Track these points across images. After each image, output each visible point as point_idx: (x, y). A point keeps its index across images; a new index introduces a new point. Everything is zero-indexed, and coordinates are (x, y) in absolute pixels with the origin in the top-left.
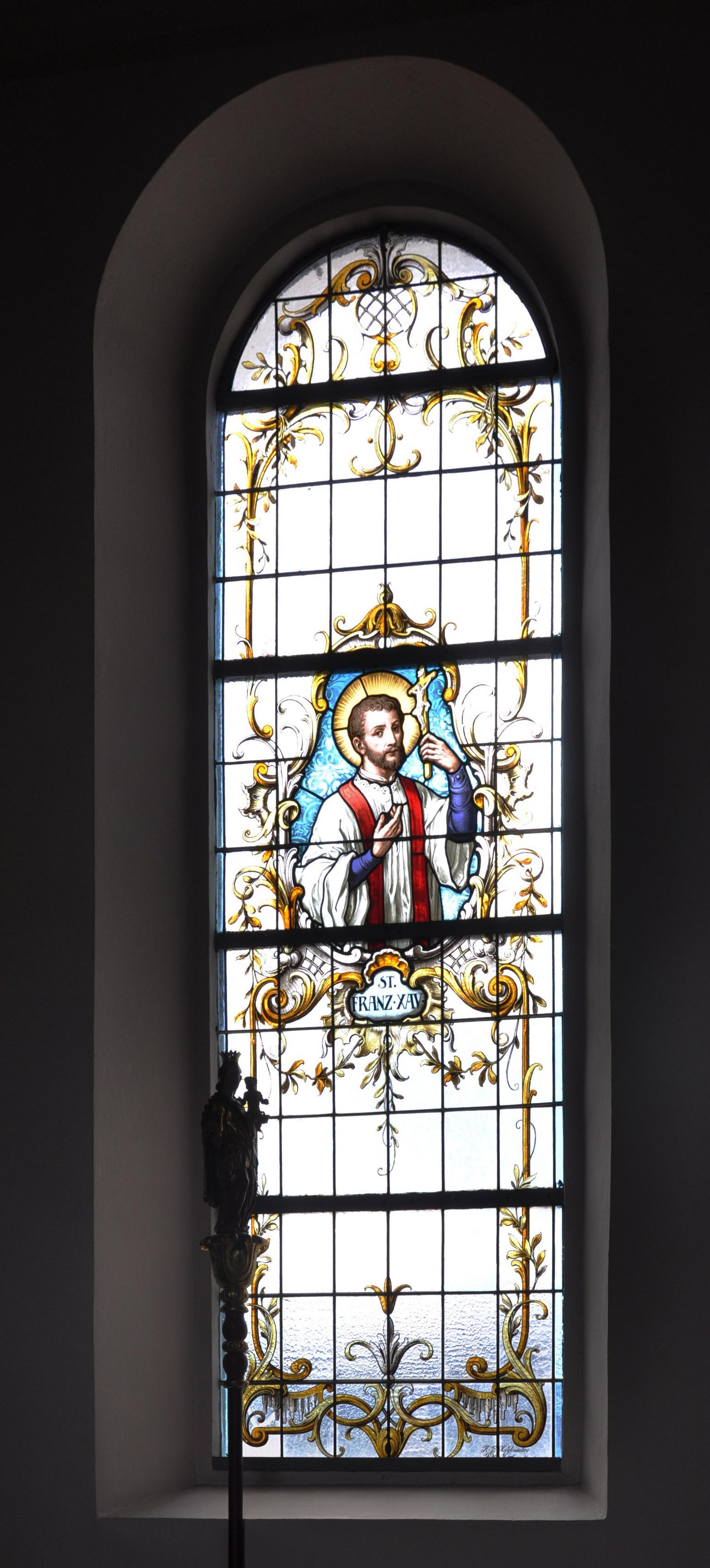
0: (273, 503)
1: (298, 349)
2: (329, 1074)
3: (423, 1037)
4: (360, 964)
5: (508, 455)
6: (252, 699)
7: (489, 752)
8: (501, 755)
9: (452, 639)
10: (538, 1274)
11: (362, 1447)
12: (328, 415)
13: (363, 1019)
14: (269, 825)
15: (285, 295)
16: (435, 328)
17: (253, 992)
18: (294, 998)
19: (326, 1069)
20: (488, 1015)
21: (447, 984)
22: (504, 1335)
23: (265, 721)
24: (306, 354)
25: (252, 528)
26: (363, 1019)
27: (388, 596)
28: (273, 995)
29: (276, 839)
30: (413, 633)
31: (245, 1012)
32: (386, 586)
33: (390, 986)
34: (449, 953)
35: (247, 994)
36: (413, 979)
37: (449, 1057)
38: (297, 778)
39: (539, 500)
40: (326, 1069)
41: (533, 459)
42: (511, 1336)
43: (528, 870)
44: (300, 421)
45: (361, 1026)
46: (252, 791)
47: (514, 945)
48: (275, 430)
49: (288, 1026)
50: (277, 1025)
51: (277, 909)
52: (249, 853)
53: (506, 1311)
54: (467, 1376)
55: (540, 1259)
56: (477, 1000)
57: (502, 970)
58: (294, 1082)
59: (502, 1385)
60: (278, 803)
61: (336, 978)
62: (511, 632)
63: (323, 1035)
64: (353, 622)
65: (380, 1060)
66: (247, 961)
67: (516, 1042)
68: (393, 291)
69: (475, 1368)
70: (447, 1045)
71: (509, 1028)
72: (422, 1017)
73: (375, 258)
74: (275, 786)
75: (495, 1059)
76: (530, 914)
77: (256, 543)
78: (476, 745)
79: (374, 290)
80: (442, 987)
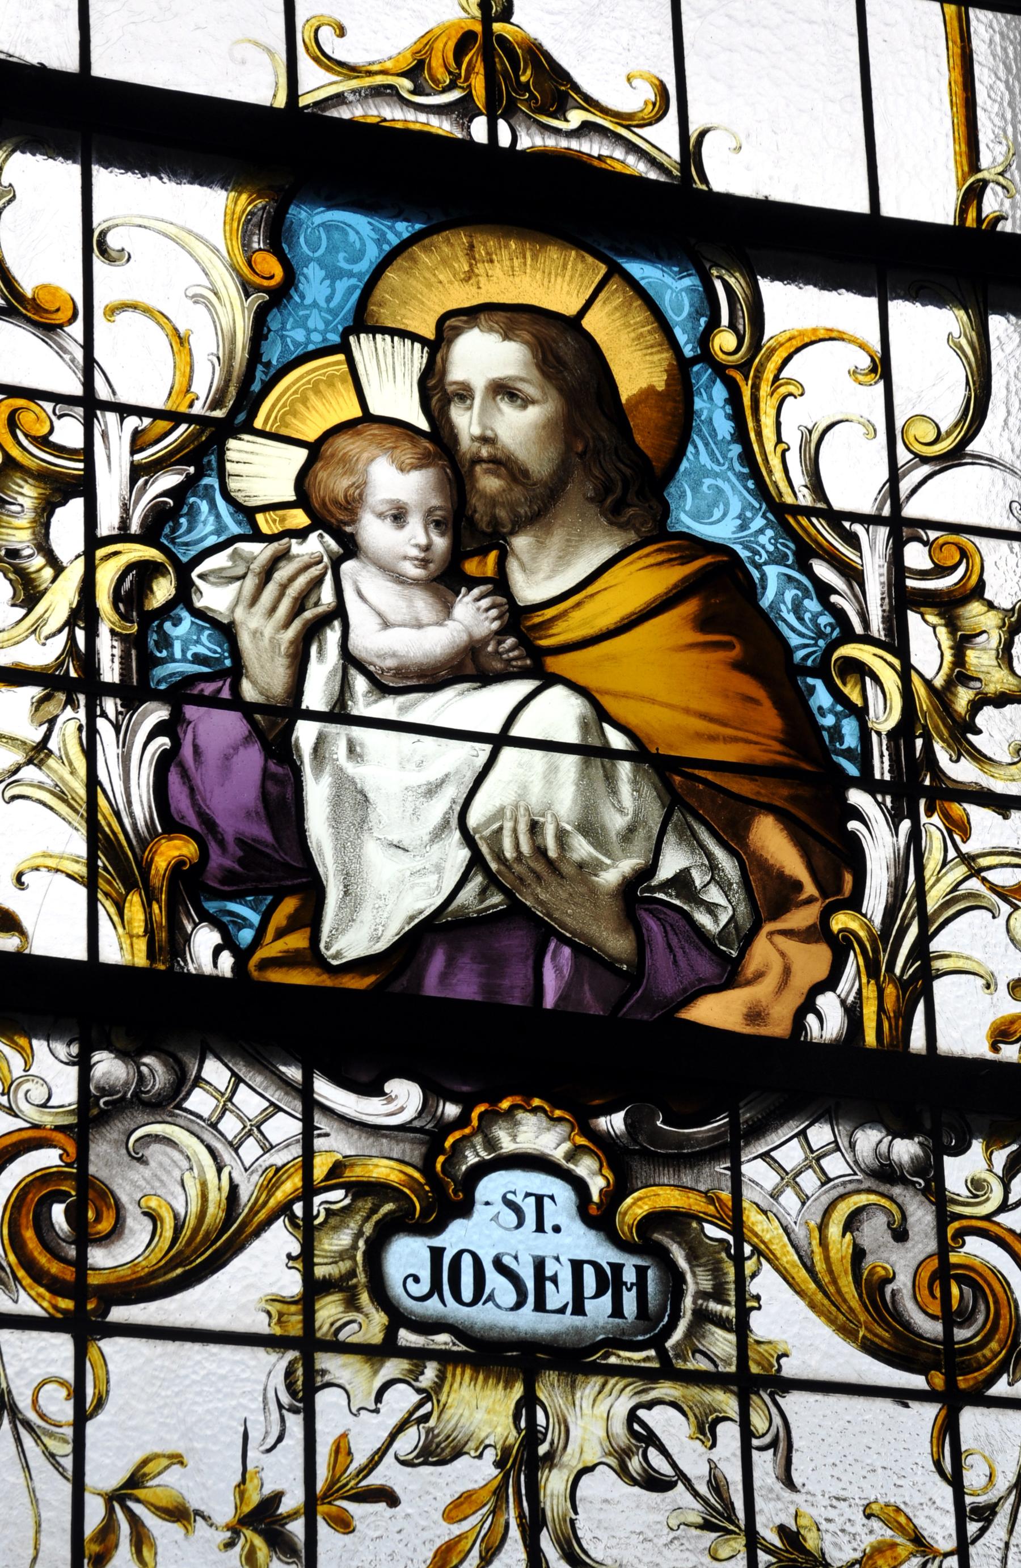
2: (292, 1516)
3: (663, 1421)
7: (874, 544)
8: (916, 556)
9: (727, 174)
14: (61, 598)
18: (153, 1216)
19: (277, 1498)
20: (917, 1382)
21: (756, 1251)
26: (427, 1327)
28: (59, 1196)
29: (89, 661)
30: (586, 129)
33: (540, 1228)
36: (636, 1207)
37: (772, 1513)
38: (168, 480)
40: (277, 1498)
45: (418, 1356)
49: (119, 1314)
51: (91, 883)
56: (870, 1315)
57: (961, 1234)
58: (140, 1538)
60: (93, 542)
61: (321, 1168)
63: (269, 1368)
65: (502, 1487)
72: (662, 1354)
74: (85, 487)
75: (951, 1544)
78: (835, 518)
80: (739, 1260)
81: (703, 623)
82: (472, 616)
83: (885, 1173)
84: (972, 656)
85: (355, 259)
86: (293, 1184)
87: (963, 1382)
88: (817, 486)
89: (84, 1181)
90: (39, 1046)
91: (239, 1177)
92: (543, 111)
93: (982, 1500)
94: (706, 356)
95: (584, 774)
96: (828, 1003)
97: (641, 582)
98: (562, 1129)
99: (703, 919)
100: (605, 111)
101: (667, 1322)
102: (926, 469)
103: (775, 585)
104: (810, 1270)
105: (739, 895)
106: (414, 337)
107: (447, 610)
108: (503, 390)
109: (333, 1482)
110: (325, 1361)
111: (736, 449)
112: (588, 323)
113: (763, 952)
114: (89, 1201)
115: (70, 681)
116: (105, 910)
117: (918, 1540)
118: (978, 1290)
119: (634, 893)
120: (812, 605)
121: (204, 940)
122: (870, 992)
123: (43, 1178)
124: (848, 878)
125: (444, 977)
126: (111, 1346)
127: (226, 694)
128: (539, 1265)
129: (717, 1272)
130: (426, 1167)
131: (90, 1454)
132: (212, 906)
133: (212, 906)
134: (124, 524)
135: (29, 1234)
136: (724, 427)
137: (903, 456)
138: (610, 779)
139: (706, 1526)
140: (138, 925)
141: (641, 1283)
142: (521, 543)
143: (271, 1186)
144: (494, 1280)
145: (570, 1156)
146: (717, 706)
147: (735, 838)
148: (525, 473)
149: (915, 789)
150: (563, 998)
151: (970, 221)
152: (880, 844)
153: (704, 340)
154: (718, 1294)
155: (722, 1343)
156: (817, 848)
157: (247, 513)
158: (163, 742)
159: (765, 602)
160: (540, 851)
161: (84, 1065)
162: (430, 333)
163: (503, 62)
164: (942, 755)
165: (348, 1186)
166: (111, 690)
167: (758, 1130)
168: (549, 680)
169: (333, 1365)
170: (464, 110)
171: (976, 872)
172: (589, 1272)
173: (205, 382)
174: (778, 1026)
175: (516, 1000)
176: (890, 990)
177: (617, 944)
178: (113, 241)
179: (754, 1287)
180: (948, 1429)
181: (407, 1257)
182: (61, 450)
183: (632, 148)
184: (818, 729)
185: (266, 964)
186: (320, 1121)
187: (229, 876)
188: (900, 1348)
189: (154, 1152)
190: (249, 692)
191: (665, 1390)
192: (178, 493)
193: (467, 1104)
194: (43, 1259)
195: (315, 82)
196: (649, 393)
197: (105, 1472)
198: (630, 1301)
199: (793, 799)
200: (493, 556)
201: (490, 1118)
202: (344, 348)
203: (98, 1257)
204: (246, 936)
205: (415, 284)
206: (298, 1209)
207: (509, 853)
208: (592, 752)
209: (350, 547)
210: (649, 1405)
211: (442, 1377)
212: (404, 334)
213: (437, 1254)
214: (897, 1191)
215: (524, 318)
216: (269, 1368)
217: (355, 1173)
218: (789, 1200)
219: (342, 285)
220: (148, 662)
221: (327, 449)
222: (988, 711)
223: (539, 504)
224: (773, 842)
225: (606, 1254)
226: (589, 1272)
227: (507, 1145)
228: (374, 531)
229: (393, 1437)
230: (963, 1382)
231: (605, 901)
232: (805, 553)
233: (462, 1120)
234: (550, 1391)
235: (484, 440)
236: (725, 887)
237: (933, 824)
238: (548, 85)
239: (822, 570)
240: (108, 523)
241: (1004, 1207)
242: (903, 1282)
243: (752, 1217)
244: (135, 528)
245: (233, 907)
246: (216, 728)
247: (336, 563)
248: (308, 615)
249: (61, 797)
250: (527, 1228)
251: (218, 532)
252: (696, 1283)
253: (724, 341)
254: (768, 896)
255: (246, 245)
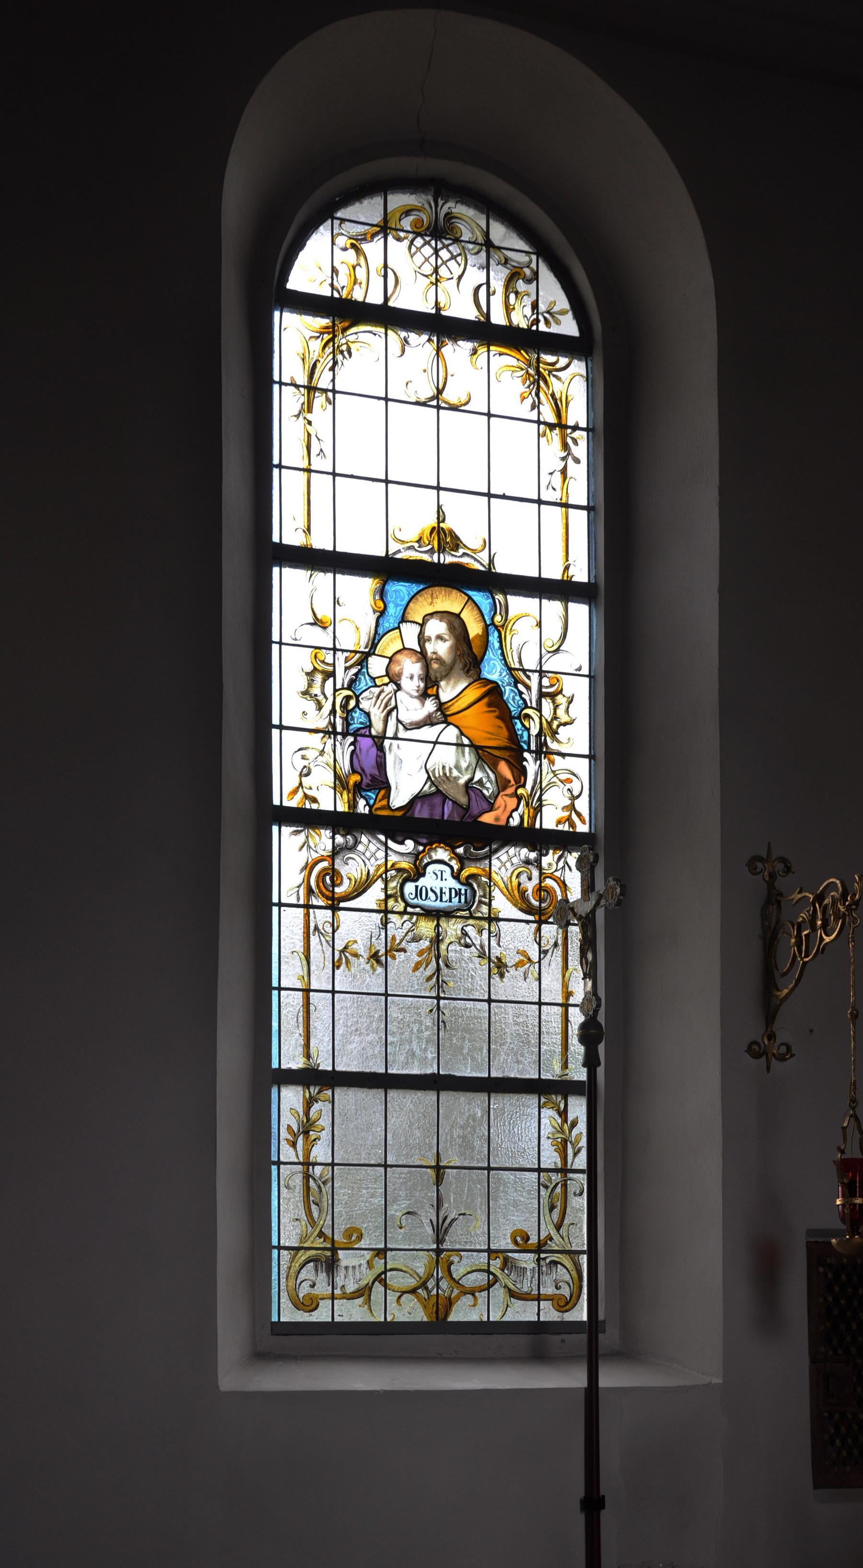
0: (330, 403)
1: (354, 268)
3: (470, 930)
4: (416, 856)
5: (549, 416)
6: (310, 587)
7: (535, 677)
8: (545, 682)
9: (502, 567)
10: (575, 1154)
11: (411, 1311)
12: (383, 336)
13: (414, 907)
14: (327, 707)
15: (339, 214)
16: (480, 286)
17: (308, 868)
18: (350, 879)
19: (378, 951)
20: (531, 918)
22: (545, 1210)
23: (325, 612)
24: (361, 273)
25: (310, 423)
26: (414, 907)
27: (441, 516)
28: (327, 874)
29: (334, 726)
30: (464, 554)
31: (299, 887)
32: (439, 507)
34: (497, 856)
35: (302, 871)
36: (465, 873)
38: (354, 670)
39: (577, 461)
40: (378, 951)
41: (571, 423)
42: (552, 1208)
43: (569, 790)
44: (356, 333)
45: (412, 914)
46: (310, 675)
47: (556, 856)
48: (331, 336)
49: (342, 905)
50: (330, 902)
52: (307, 733)
53: (546, 1187)
54: (512, 1246)
55: (578, 1141)
57: (545, 878)
59: (543, 1256)
60: (335, 690)
61: (389, 866)
62: (553, 572)
63: (377, 918)
64: (411, 535)
66: (302, 837)
67: (556, 945)
68: (444, 241)
69: (519, 1239)
70: (493, 943)
71: (550, 931)
73: (427, 206)
74: (333, 674)
75: (537, 960)
76: (571, 830)
77: (314, 440)
78: (524, 671)
79: (426, 235)
80: (490, 887)
81: (489, 705)
82: (430, 706)
83: (527, 862)
84: (558, 711)
85: (402, 601)
86: (383, 869)
87: (543, 918)
88: (520, 662)
89: (333, 870)
90: (322, 831)
91: (370, 868)
92: (452, 550)
93: (546, 948)
94: (493, 624)
95: (457, 751)
96: (516, 815)
97: (473, 694)
98: (447, 853)
99: (485, 792)
100: (469, 549)
101: (471, 904)
102: (550, 655)
103: (508, 693)
104: (507, 889)
105: (495, 785)
106: (417, 623)
107: (423, 704)
108: (439, 637)
109: (391, 947)
110: (389, 916)
111: (500, 651)
112: (462, 616)
113: (500, 801)
114: (334, 873)
115: (330, 732)
116: (338, 795)
117: (529, 959)
118: (548, 892)
119: (468, 785)
120: (518, 698)
121: (362, 803)
122: (526, 811)
123: (324, 869)
124: (523, 779)
125: (420, 811)
126: (341, 914)
127: (367, 733)
128: (441, 889)
129: (484, 890)
130: (415, 864)
131: (336, 941)
132: (363, 794)
133: (363, 794)
134: (343, 685)
135: (321, 884)
136: (497, 645)
137: (544, 651)
138: (463, 752)
139: (479, 957)
140: (346, 800)
141: (466, 894)
142: (443, 683)
143: (377, 870)
144: (431, 894)
145: (450, 860)
146: (491, 730)
147: (494, 768)
148: (444, 662)
149: (542, 751)
150: (449, 816)
151: (565, 578)
152: (531, 767)
153: (493, 619)
154: (484, 896)
155: (485, 909)
156: (515, 770)
157: (373, 679)
158: (352, 748)
159: (505, 698)
160: (445, 774)
161: (333, 838)
162: (421, 622)
163: (442, 535)
164: (549, 740)
165: (396, 870)
166: (339, 734)
167: (496, 851)
168: (449, 724)
169: (393, 917)
170: (431, 552)
171: (555, 775)
172: (453, 891)
173: (363, 643)
174: (502, 822)
175: (437, 817)
176: (531, 810)
177: (463, 800)
178: (341, 601)
179: (493, 894)
180: (539, 930)
181: (410, 888)
182: (327, 664)
183: (476, 560)
184: (517, 735)
185: (377, 809)
186: (389, 852)
187: (368, 785)
188: (528, 909)
189: (350, 861)
190: (374, 732)
191: (471, 922)
192: (356, 675)
193: (425, 845)
194: (324, 891)
195: (393, 547)
196: (478, 635)
197: (339, 945)
198: (463, 898)
199: (510, 756)
200: (435, 688)
201: (431, 849)
202: (399, 628)
203: (337, 890)
204: (372, 802)
205: (417, 607)
206: (384, 876)
207: (437, 775)
208: (459, 745)
209: (399, 688)
210: (466, 926)
211: (417, 919)
212: (414, 622)
213: (417, 887)
214: (530, 867)
215: (445, 615)
216: (377, 918)
217: (397, 866)
218: (503, 869)
219: (399, 609)
220: (348, 724)
221: (394, 659)
222: (562, 727)
223: (448, 672)
224: (504, 769)
225: (458, 886)
226: (453, 891)
227: (435, 857)
228: (405, 682)
229: (406, 935)
230: (543, 918)
231: (461, 788)
232: (517, 682)
233: (424, 851)
234: (443, 923)
235: (434, 653)
236: (491, 782)
237: (545, 762)
238: (454, 542)
239: (520, 687)
240: (339, 686)
241: (556, 870)
242: (530, 892)
243: (494, 875)
244: (345, 686)
245: (369, 794)
246: (365, 743)
247: (395, 692)
248: (388, 708)
249: (327, 765)
250: (439, 881)
251: (367, 684)
252: (479, 893)
253: (498, 618)
254: (502, 785)
255: (374, 598)
